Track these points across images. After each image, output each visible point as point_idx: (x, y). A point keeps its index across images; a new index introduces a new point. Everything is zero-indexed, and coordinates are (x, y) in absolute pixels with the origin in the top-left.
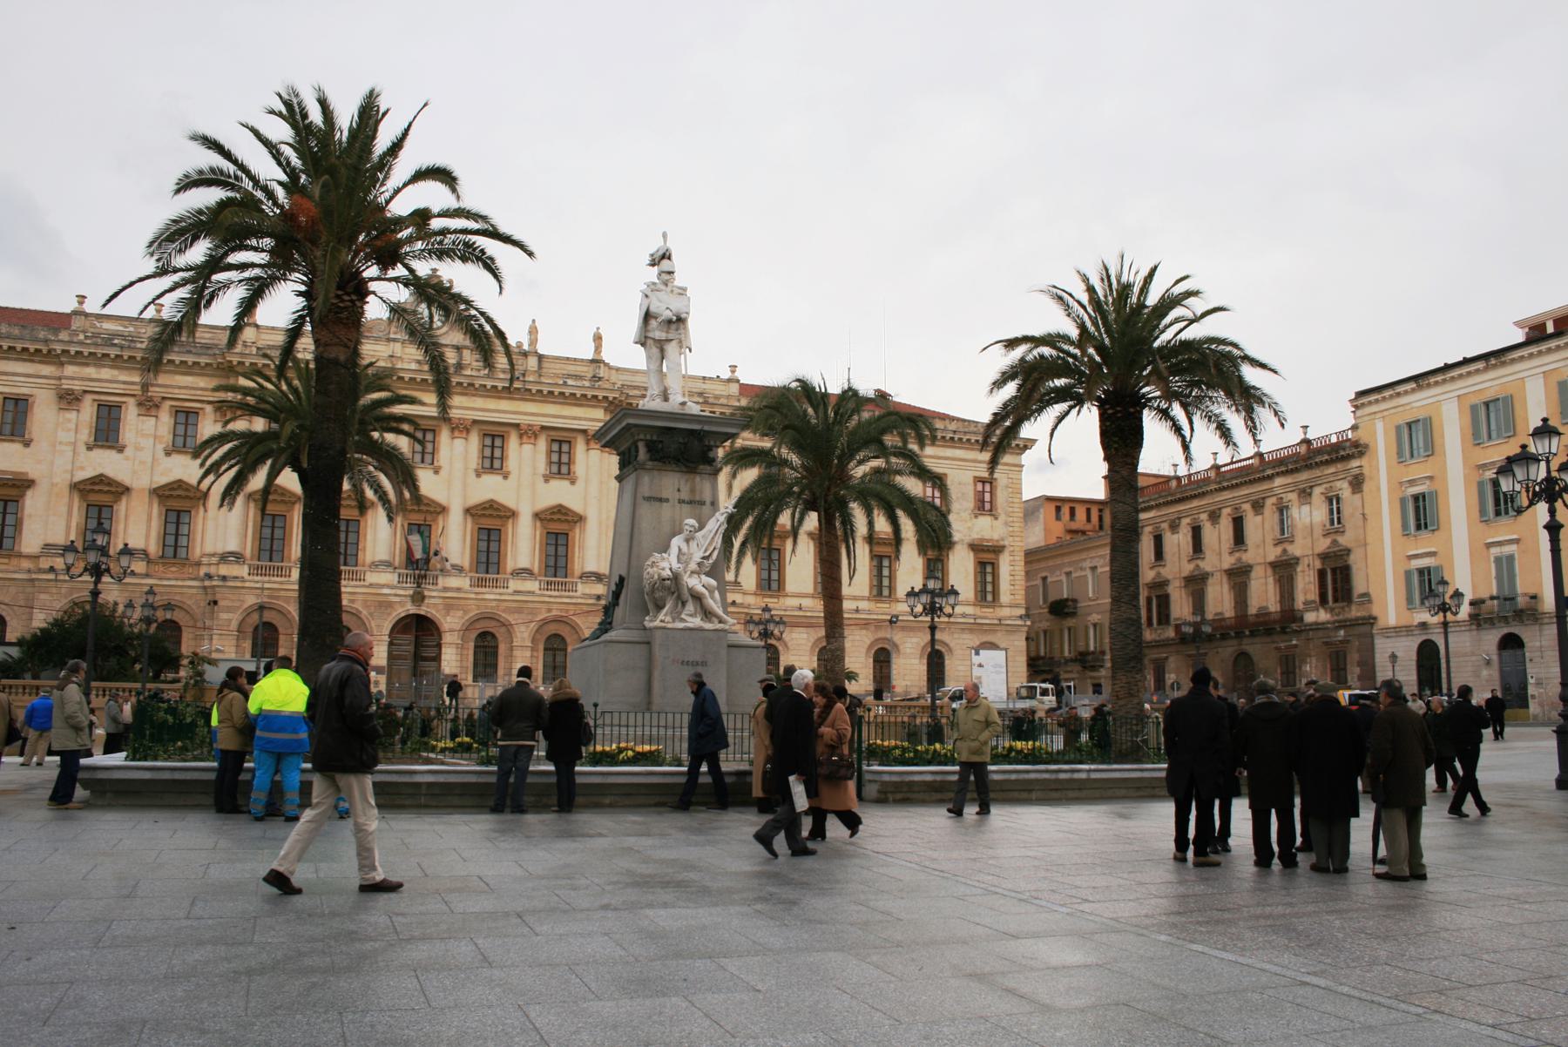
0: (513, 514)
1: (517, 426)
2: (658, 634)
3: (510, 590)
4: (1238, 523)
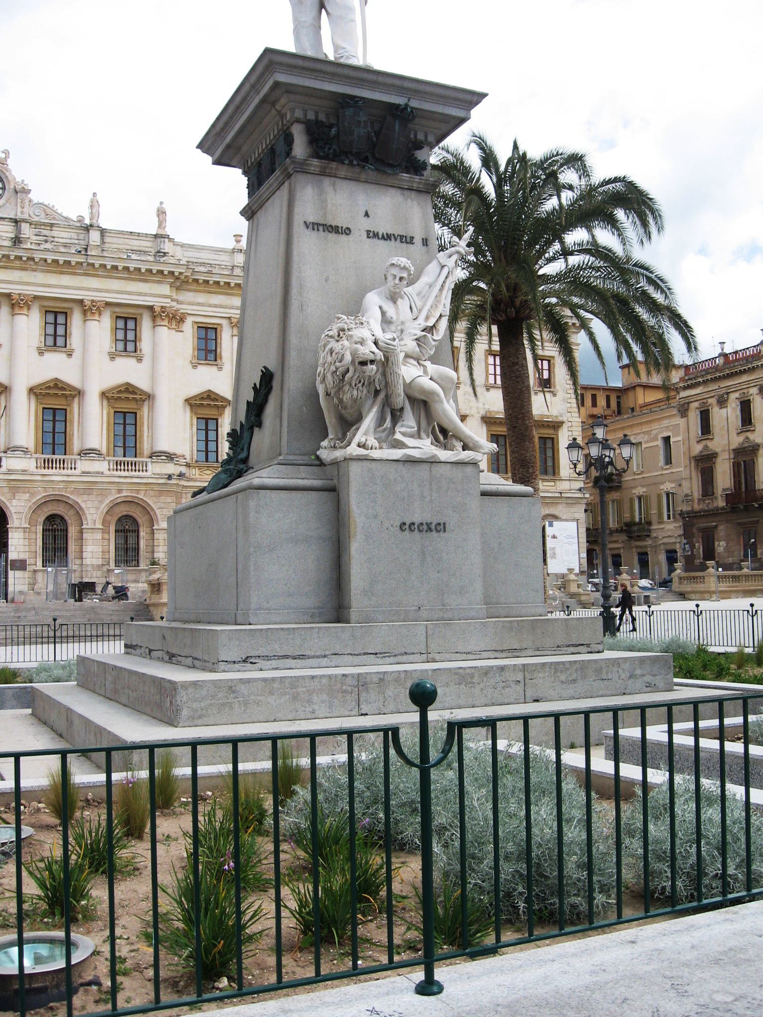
0: (79, 393)
1: (81, 302)
2: (355, 469)
3: (78, 472)
4: (705, 416)
